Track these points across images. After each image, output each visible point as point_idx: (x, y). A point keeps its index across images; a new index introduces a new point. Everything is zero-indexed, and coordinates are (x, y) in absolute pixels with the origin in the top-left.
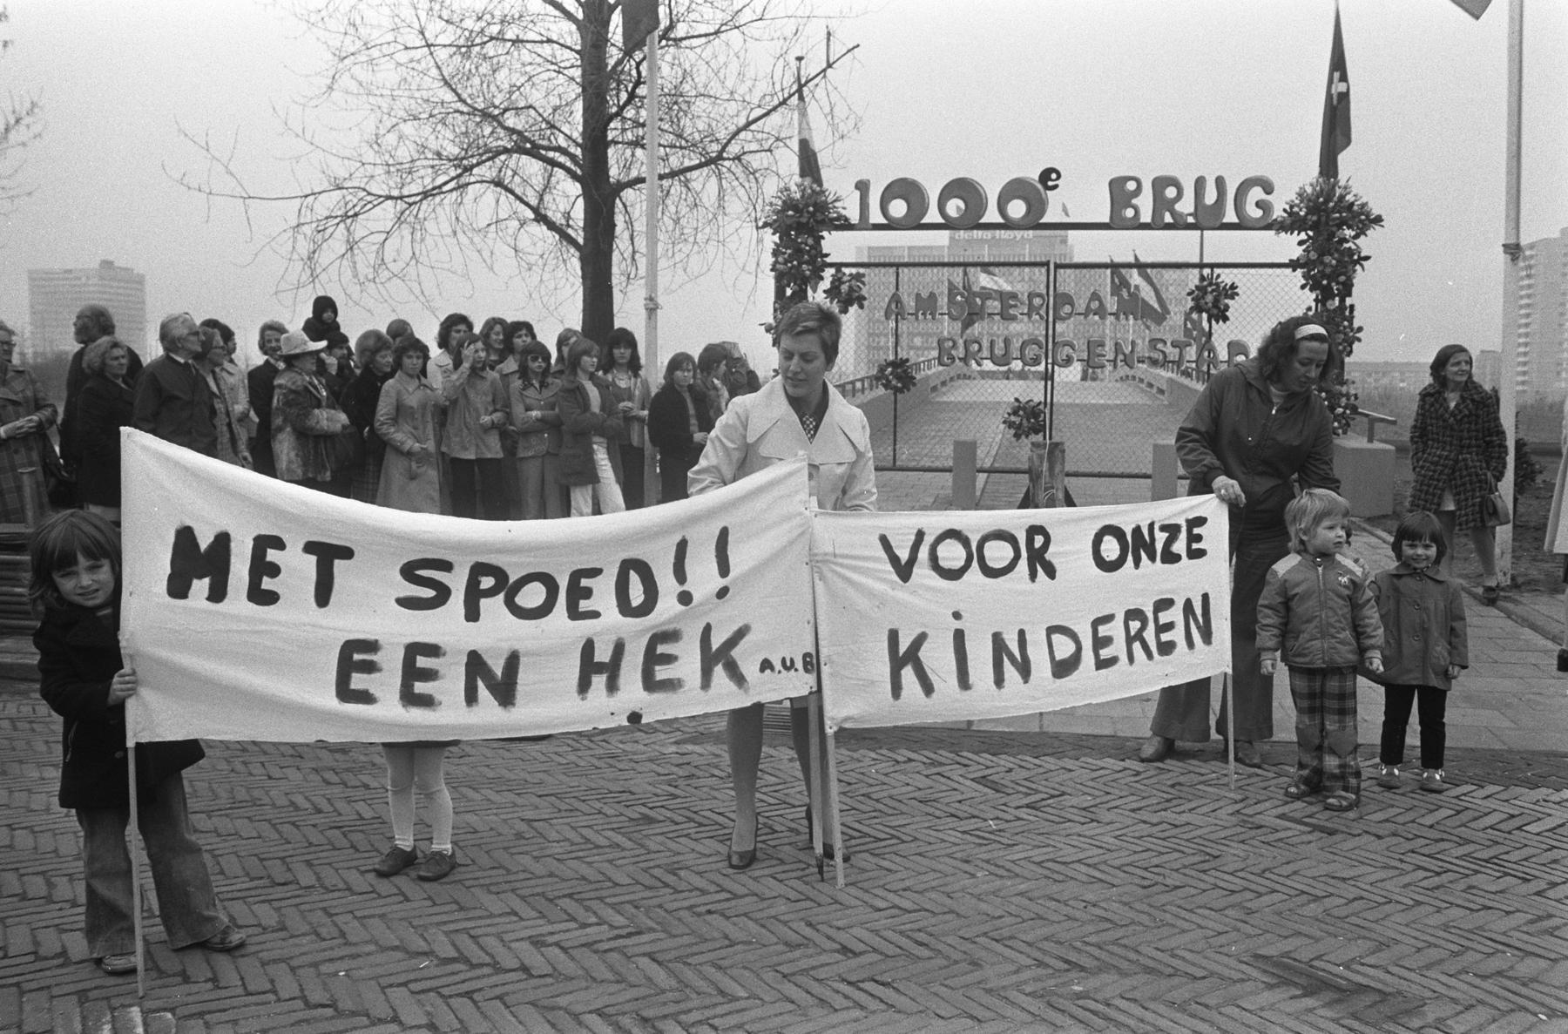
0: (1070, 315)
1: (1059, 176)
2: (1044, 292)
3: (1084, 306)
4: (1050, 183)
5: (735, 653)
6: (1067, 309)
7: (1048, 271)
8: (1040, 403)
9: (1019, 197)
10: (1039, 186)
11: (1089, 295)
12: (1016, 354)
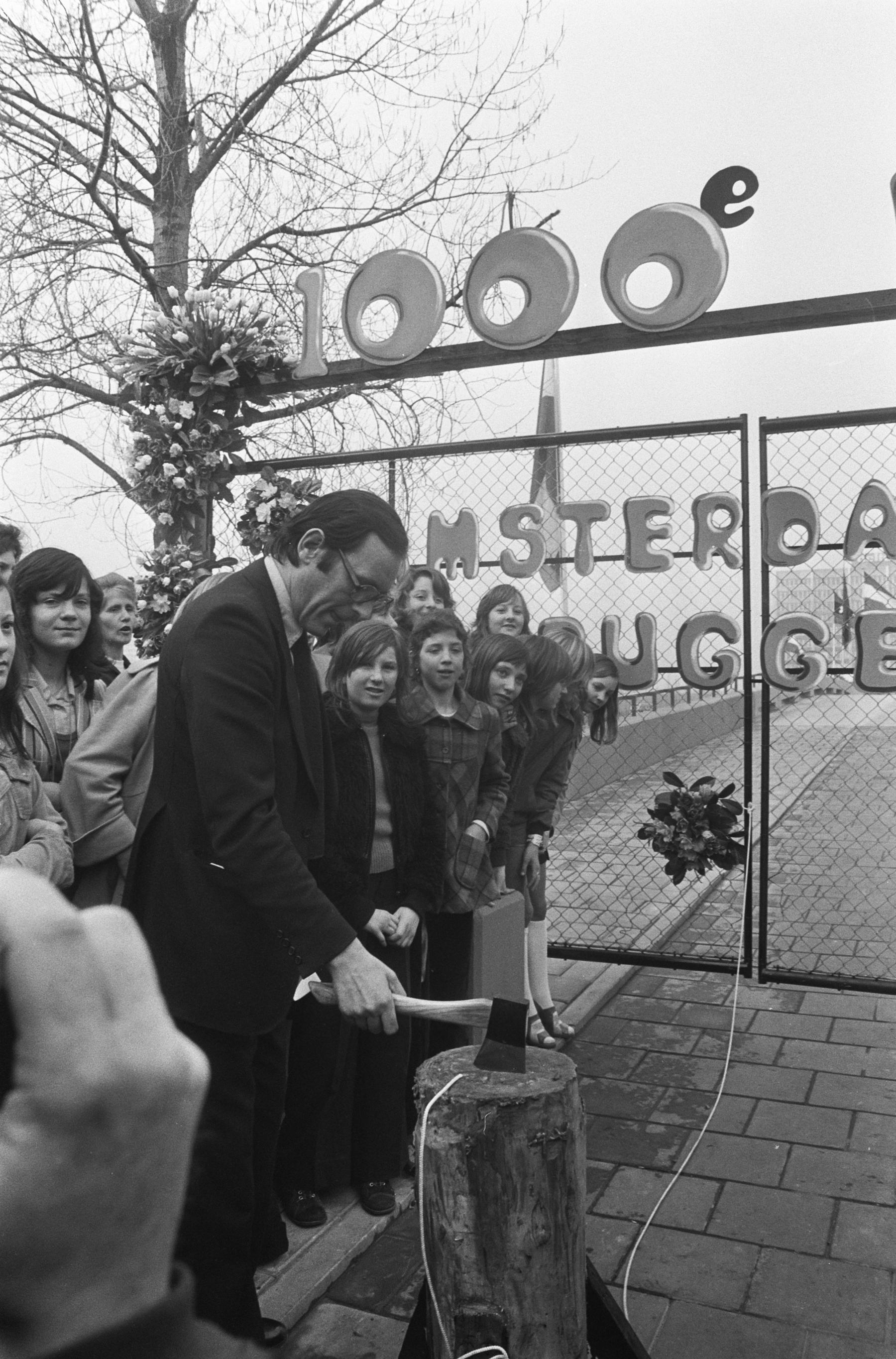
0: (803, 552)
1: (752, 185)
2: (738, 493)
3: (843, 525)
4: (731, 209)
5: (819, 1074)
6: (796, 535)
7: (744, 441)
8: (730, 789)
9: (653, 256)
10: (706, 222)
11: (854, 492)
12: (668, 658)
